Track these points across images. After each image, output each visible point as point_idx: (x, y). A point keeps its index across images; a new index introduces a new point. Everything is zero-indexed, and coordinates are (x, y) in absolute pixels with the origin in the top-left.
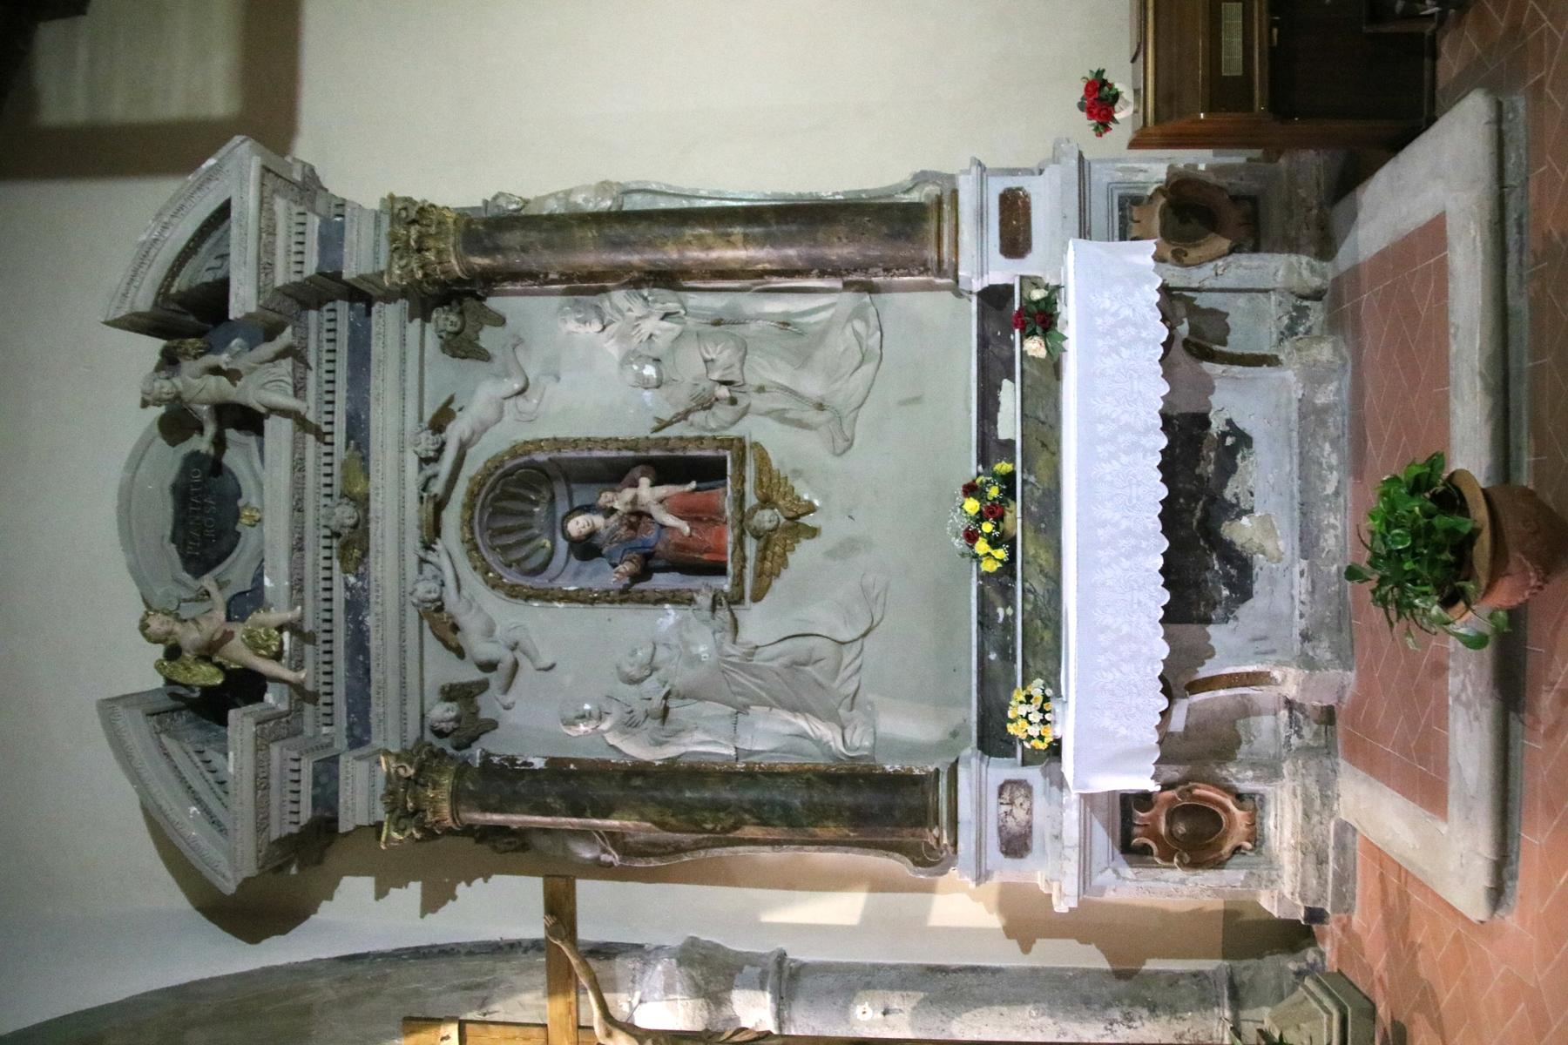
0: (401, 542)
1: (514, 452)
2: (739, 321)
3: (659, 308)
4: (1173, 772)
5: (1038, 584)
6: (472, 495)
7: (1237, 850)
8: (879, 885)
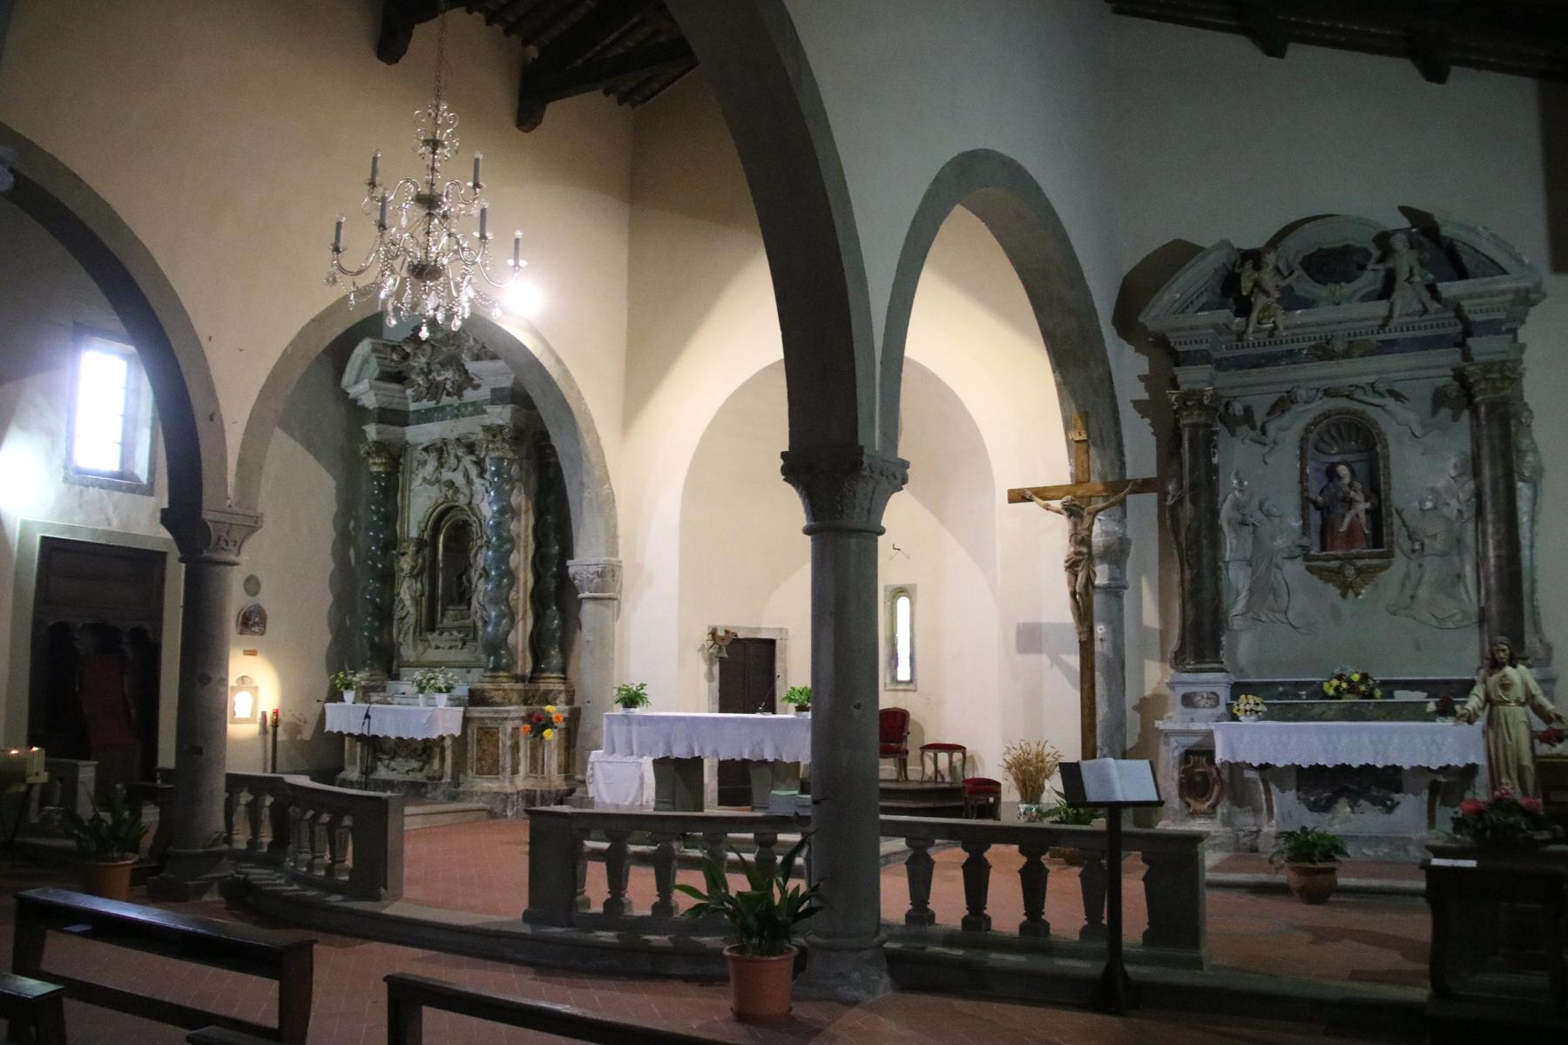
0: (1325, 378)
1: (1380, 434)
2: (1460, 553)
3: (1464, 508)
4: (1225, 774)
5: (1317, 710)
6: (1355, 413)
7: (1189, 805)
8: (1164, 635)
